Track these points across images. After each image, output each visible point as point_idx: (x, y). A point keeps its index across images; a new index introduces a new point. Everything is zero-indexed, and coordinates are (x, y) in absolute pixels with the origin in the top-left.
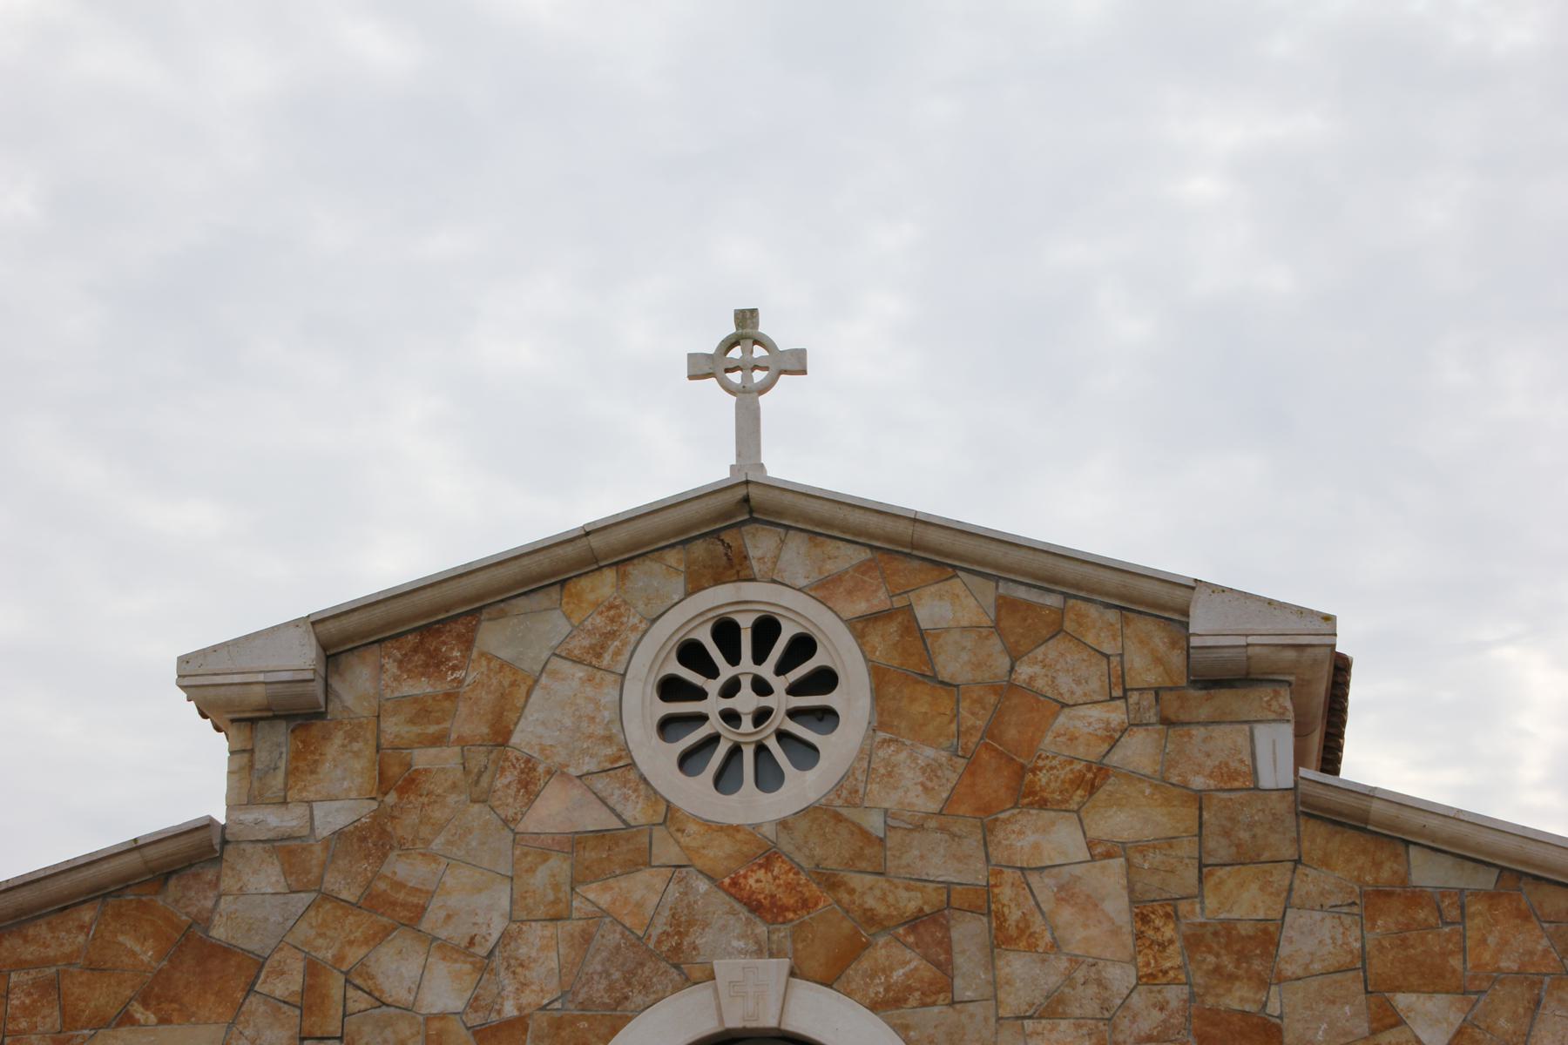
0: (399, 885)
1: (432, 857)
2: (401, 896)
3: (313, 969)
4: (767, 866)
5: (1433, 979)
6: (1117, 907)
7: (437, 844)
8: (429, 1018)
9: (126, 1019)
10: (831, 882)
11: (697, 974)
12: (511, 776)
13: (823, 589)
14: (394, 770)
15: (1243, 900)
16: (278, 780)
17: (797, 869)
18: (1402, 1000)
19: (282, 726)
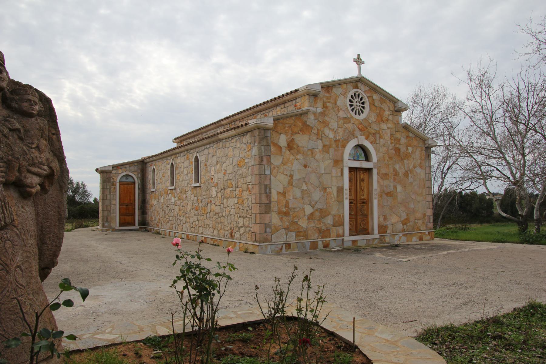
3: (318, 130)
5: (410, 146)
6: (389, 135)
9: (299, 133)
10: (367, 128)
13: (365, 92)
15: (398, 136)
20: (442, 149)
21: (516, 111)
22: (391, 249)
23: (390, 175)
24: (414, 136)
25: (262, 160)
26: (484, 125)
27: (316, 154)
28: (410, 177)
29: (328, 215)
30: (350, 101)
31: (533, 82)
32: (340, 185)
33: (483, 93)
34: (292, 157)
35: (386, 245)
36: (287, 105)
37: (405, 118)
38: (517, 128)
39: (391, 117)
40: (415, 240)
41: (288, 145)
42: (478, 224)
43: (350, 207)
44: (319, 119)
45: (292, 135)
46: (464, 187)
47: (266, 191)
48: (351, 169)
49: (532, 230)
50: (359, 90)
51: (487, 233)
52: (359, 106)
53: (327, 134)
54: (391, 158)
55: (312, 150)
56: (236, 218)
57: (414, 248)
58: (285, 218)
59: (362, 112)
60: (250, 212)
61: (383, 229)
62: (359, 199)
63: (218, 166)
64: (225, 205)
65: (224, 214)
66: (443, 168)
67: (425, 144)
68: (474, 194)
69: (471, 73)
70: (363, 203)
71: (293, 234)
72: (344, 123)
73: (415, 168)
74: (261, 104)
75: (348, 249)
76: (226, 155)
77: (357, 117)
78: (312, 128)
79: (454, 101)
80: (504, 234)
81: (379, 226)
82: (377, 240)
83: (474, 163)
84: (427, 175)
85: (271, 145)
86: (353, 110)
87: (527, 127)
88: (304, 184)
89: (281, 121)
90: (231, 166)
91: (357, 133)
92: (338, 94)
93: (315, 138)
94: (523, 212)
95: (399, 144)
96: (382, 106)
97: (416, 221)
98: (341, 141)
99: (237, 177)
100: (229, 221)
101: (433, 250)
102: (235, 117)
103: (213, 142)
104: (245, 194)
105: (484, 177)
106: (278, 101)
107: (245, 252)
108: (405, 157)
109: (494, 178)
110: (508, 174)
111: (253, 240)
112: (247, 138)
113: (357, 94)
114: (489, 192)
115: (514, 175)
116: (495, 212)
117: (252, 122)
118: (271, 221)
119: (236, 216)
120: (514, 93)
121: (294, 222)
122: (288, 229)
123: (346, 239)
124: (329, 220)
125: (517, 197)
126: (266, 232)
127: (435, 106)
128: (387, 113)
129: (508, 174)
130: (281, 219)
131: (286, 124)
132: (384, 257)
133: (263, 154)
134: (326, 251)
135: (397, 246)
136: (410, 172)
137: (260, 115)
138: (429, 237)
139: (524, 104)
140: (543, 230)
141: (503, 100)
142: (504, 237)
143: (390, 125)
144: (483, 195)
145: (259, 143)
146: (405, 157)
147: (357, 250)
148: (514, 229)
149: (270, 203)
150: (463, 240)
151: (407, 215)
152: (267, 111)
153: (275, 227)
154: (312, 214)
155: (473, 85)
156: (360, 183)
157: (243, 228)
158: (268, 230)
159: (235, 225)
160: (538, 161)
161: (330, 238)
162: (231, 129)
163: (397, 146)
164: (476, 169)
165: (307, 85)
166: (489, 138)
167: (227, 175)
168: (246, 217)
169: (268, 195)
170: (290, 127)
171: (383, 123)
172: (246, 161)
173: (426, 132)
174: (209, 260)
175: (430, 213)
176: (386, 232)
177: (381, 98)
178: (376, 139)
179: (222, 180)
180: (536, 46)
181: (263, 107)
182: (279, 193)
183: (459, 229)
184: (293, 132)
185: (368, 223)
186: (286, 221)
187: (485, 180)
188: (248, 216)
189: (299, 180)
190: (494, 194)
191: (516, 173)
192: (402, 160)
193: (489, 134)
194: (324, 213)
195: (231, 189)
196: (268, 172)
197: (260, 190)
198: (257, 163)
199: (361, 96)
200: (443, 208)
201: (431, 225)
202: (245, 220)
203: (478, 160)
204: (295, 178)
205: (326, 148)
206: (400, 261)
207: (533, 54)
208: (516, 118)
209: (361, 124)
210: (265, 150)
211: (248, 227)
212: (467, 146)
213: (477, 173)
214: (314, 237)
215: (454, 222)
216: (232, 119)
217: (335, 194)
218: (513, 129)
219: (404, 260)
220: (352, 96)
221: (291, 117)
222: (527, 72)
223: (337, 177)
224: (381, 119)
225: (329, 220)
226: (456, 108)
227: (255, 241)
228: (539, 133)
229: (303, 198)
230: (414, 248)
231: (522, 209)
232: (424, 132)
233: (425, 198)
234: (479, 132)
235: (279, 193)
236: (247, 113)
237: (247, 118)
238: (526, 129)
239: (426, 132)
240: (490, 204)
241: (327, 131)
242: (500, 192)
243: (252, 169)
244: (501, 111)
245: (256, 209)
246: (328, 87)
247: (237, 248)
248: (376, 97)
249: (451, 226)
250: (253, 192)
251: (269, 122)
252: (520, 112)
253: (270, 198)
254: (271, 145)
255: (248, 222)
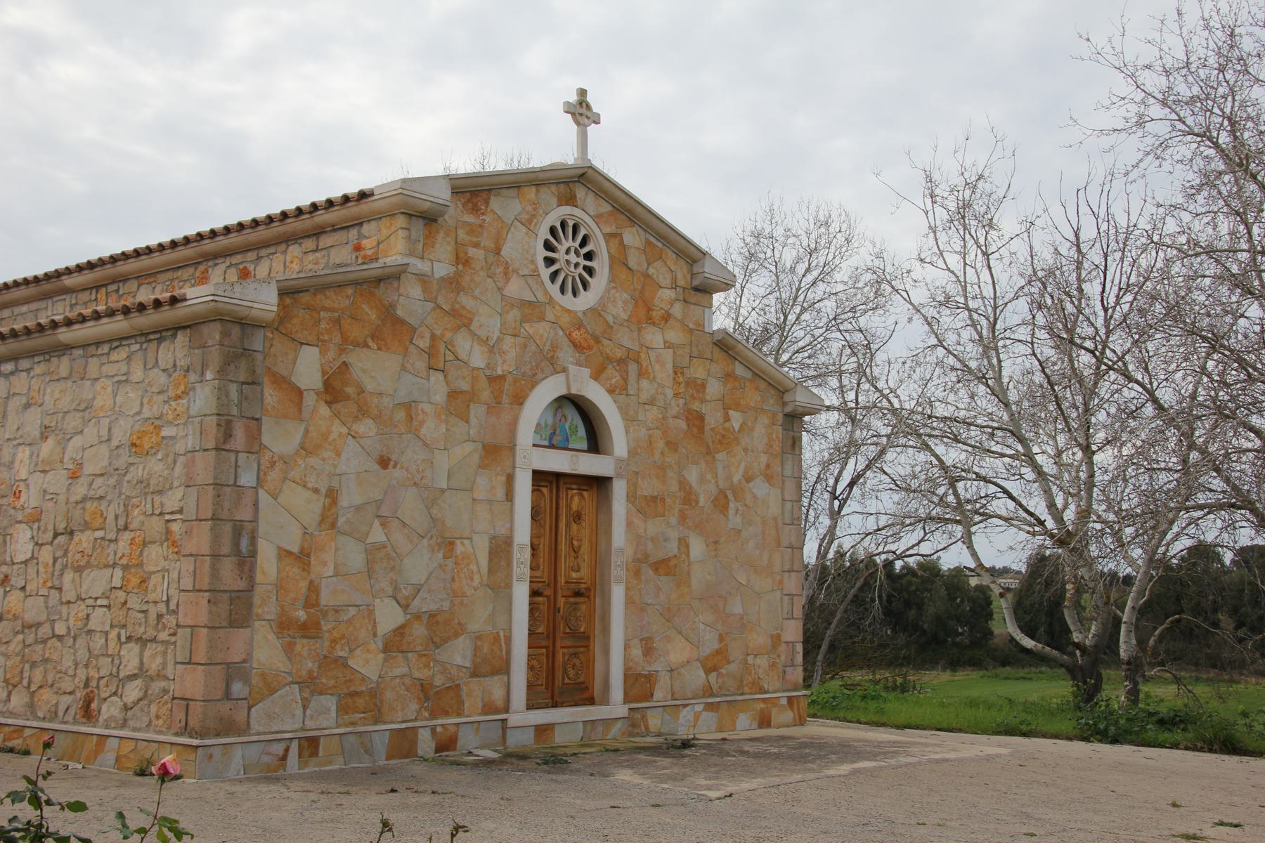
0: (464, 308)
1: (476, 298)
2: (464, 313)
3: (433, 337)
4: (579, 329)
5: (737, 407)
6: (669, 367)
7: (477, 292)
8: (474, 369)
9: (366, 345)
10: (598, 341)
11: (558, 369)
12: (500, 269)
13: (597, 218)
14: (461, 255)
15: (698, 371)
16: (420, 247)
17: (587, 332)
18: (731, 412)
19: (421, 222)
20: (834, 416)
21: (1070, 308)
22: (666, 755)
23: (668, 500)
24: (749, 375)
25: (228, 435)
26: (970, 346)
27: (422, 423)
28: (731, 512)
29: (457, 635)
30: (548, 246)
31: (1122, 222)
32: (502, 530)
33: (970, 242)
34: (337, 429)
35: (650, 740)
36: (326, 241)
37: (722, 315)
38: (1071, 361)
39: (677, 310)
40: (744, 725)
41: (327, 384)
42: (944, 669)
43: (533, 609)
44: (441, 300)
45: (342, 350)
46: (900, 547)
47: (236, 544)
48: (541, 478)
49: (1115, 693)
50: (577, 212)
51: (973, 704)
52: (577, 265)
53: (463, 356)
54: (672, 445)
55: (409, 407)
56: (113, 644)
57: (743, 753)
58: (303, 647)
59: (585, 285)
60: (170, 620)
61: (639, 686)
62: (562, 580)
63: (47, 448)
64: (71, 596)
65: (60, 629)
66: (837, 481)
67: (784, 404)
68: (929, 569)
69: (936, 176)
70: (577, 594)
71: (330, 702)
72: (525, 319)
73: (749, 480)
74: (227, 230)
75: (523, 757)
76: (86, 408)
77: (567, 301)
78: (414, 330)
79: (877, 263)
80: (1028, 707)
81: (626, 676)
82: (619, 725)
83: (935, 470)
84: (788, 506)
85: (266, 381)
86: (554, 276)
87: (1100, 361)
88: (377, 522)
89: (305, 298)
90: (104, 450)
91: (566, 355)
92: (508, 217)
93: (421, 365)
94: (1085, 635)
95: (703, 401)
96: (651, 271)
97: (750, 659)
98: (509, 378)
99: (125, 489)
100: (82, 654)
101: (804, 759)
102: (122, 268)
103: (31, 354)
104: (155, 556)
105: (966, 516)
106: (292, 225)
107: (142, 773)
108: (720, 442)
109: (994, 520)
110: (1042, 511)
111: (178, 726)
112: (176, 351)
113: (571, 223)
114: (981, 565)
115: (1057, 516)
116: (996, 631)
117: (198, 295)
118: (250, 654)
119: (113, 634)
120: (1064, 251)
121: (336, 660)
122: (310, 686)
123: (514, 719)
124: (459, 654)
125: (1069, 586)
126: (227, 695)
127: (815, 273)
128: (667, 294)
129: (1042, 511)
130: (289, 649)
131: (324, 309)
132: (646, 782)
133: (235, 411)
134: (443, 762)
135: (686, 744)
136: (734, 493)
137: (223, 267)
138: (789, 716)
139: (1093, 289)
140: (1148, 696)
141: (1030, 271)
142: (1029, 718)
143: (675, 335)
144: (958, 572)
145: (222, 372)
146: (720, 442)
147: (552, 759)
148: (1058, 689)
149: (251, 588)
150: (898, 727)
151: (721, 638)
152: (251, 256)
153: (263, 675)
154: (400, 631)
155: (941, 214)
156: (568, 525)
157: (138, 682)
158: (238, 688)
159: (103, 672)
160: (1131, 471)
161: (459, 715)
162: (111, 313)
163: (695, 406)
164: (941, 491)
165: (404, 181)
166: (982, 389)
167: (84, 480)
168: (154, 640)
169: (246, 562)
170: (337, 322)
171: (651, 329)
172: (163, 434)
173: (785, 357)
174: (78, 807)
175: (793, 632)
176: (649, 696)
177: (648, 243)
178: (625, 380)
179: (62, 498)
180: (1134, 109)
181: (234, 239)
182: (283, 554)
183: (886, 688)
184: (345, 340)
185: (590, 663)
186: (307, 654)
187: (967, 524)
188: (163, 636)
189: (359, 509)
190: (993, 571)
191: (1066, 506)
192: (709, 452)
193: (982, 379)
194: (441, 627)
195: (100, 534)
196: (247, 479)
197: (216, 538)
198: (211, 445)
199: (582, 232)
200: (833, 614)
201: (797, 674)
202: (147, 653)
203: (949, 462)
204: (344, 502)
205: (458, 403)
206: (701, 798)
207: (1124, 134)
208: (1068, 331)
209: (580, 326)
210: (243, 397)
211: (161, 676)
212: (912, 412)
213: (942, 501)
214: (404, 711)
215: (868, 663)
216: (110, 270)
217: (484, 562)
218: (1058, 366)
219: (713, 794)
220: (553, 231)
221: (341, 286)
222: (1106, 188)
223: (490, 502)
224: (645, 314)
225: (459, 654)
226: (882, 284)
227: (186, 730)
228: (1137, 382)
229: (370, 572)
230: (743, 753)
231: (1083, 622)
232: (776, 360)
233: (781, 582)
234: (953, 369)
235: (283, 554)
236: (170, 256)
237: (169, 275)
238: (1098, 368)
239: (785, 357)
240: (981, 604)
241: (463, 344)
242: (1014, 567)
243: (189, 465)
244: (1022, 305)
245: (197, 611)
246: (474, 191)
247: (109, 757)
248: (632, 237)
249: (858, 676)
250: (190, 547)
251: (263, 299)
252: (1080, 312)
253: (252, 569)
254: (266, 381)
255: (159, 660)
